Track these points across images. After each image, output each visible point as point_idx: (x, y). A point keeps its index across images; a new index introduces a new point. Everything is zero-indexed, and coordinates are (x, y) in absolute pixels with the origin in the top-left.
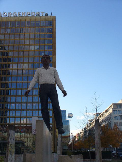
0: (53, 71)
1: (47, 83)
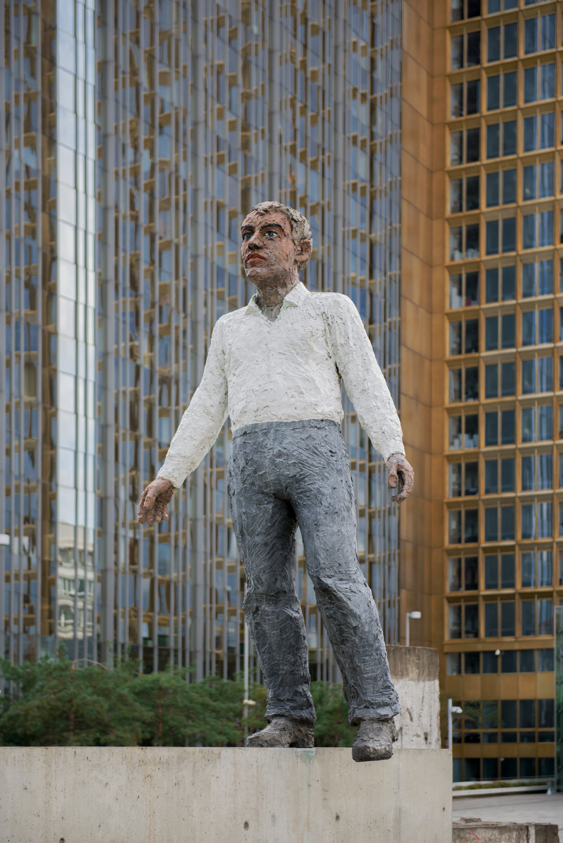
0: (319, 324)
1: (265, 418)
